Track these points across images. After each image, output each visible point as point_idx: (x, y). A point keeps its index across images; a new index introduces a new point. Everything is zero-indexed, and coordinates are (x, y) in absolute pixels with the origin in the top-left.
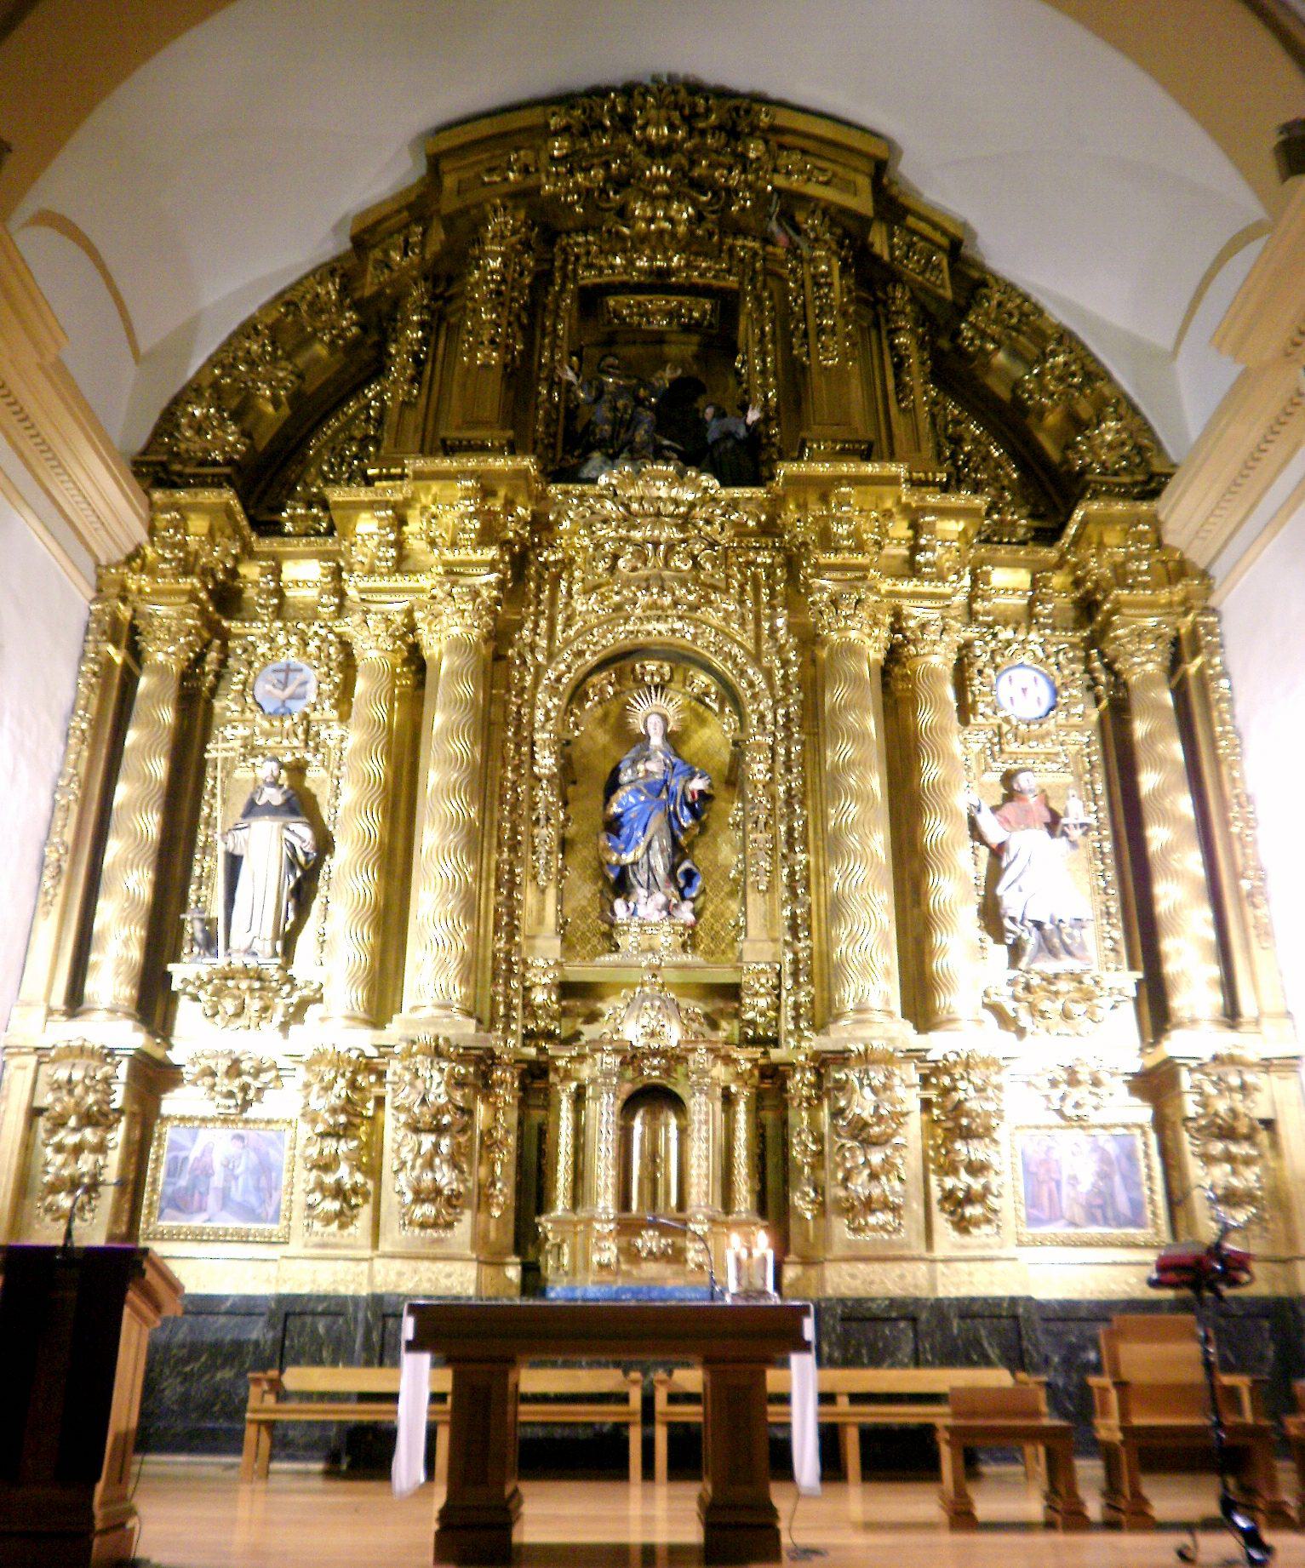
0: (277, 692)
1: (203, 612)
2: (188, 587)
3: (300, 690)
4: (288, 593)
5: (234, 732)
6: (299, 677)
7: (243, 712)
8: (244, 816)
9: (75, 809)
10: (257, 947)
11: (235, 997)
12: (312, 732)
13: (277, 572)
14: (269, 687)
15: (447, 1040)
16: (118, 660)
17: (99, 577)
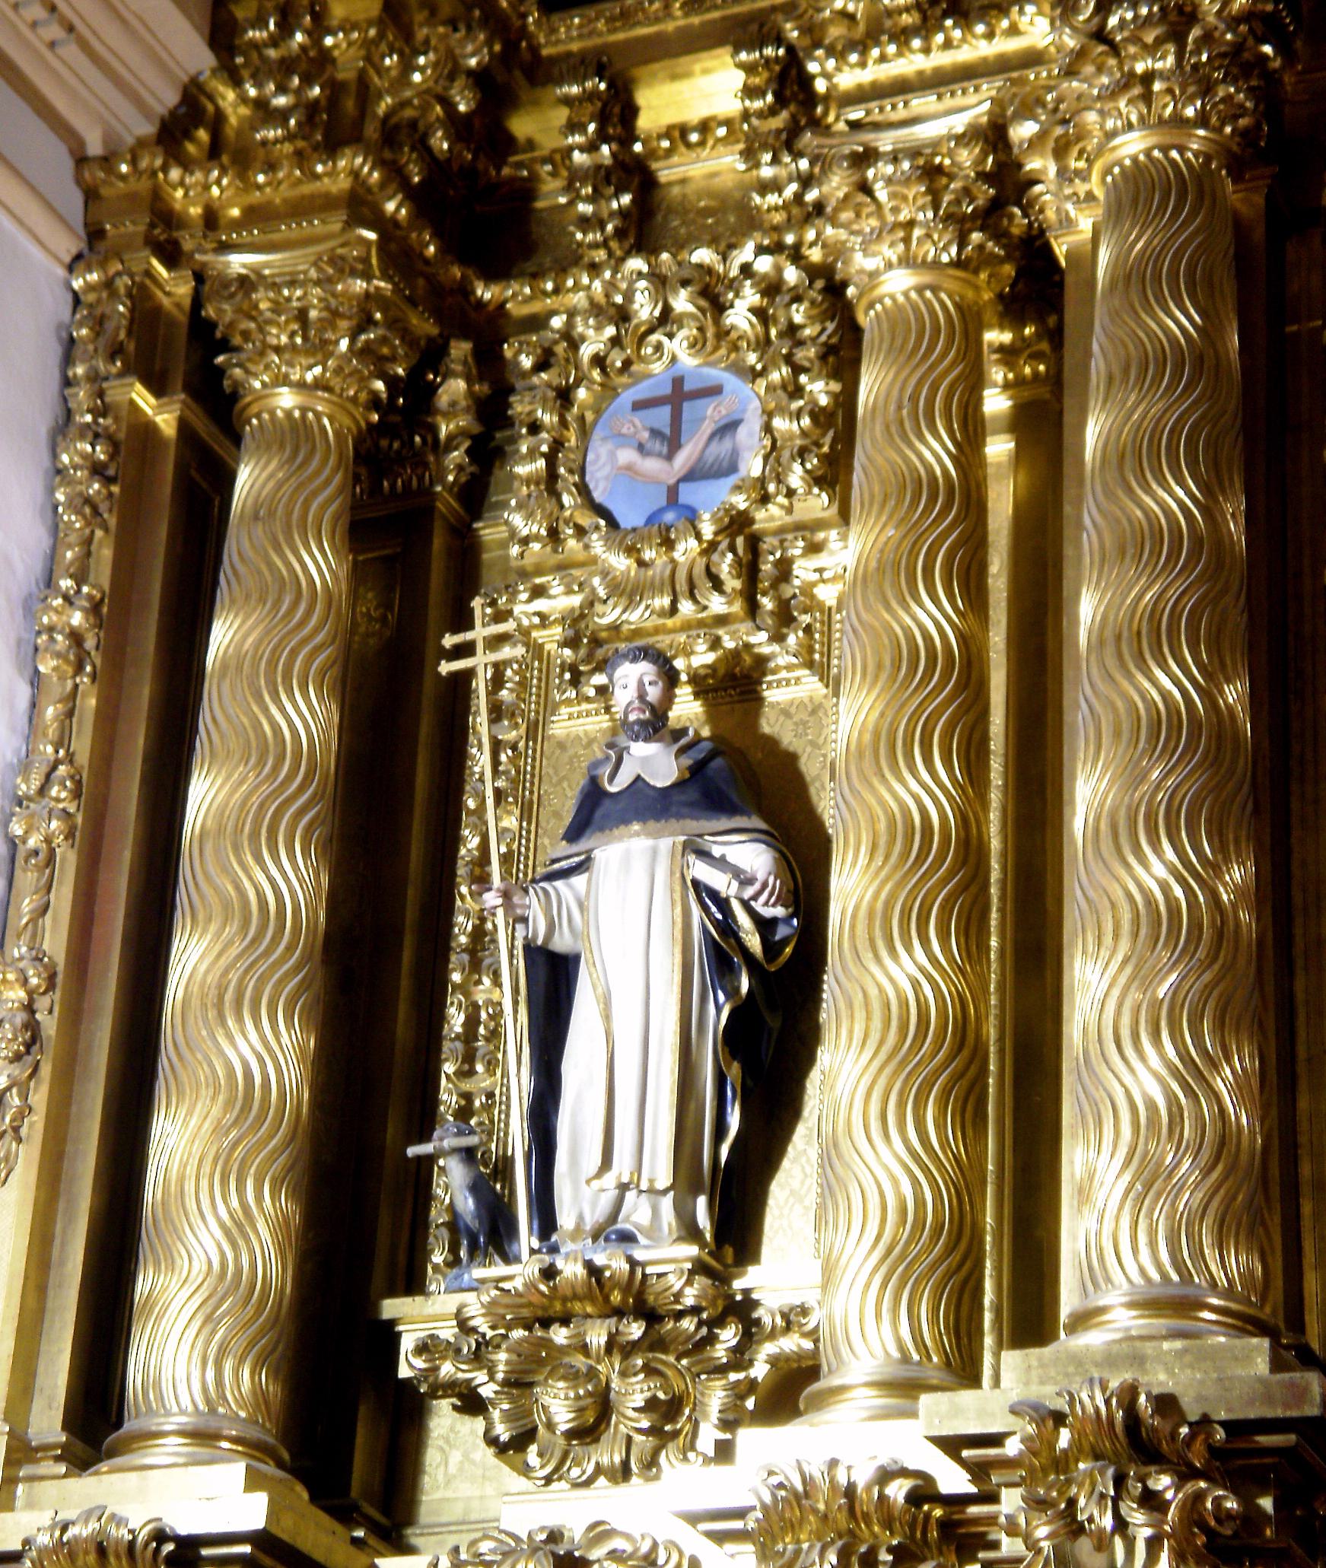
0: (652, 465)
1: (396, 254)
2: (343, 183)
3: (721, 449)
4: (665, 174)
5: (541, 605)
6: (712, 412)
7: (554, 535)
8: (574, 833)
9: (68, 859)
10: (637, 1212)
11: (573, 1377)
12: (767, 568)
13: (617, 113)
14: (627, 455)
15: (1166, 1404)
16: (166, 420)
17: (91, 195)
